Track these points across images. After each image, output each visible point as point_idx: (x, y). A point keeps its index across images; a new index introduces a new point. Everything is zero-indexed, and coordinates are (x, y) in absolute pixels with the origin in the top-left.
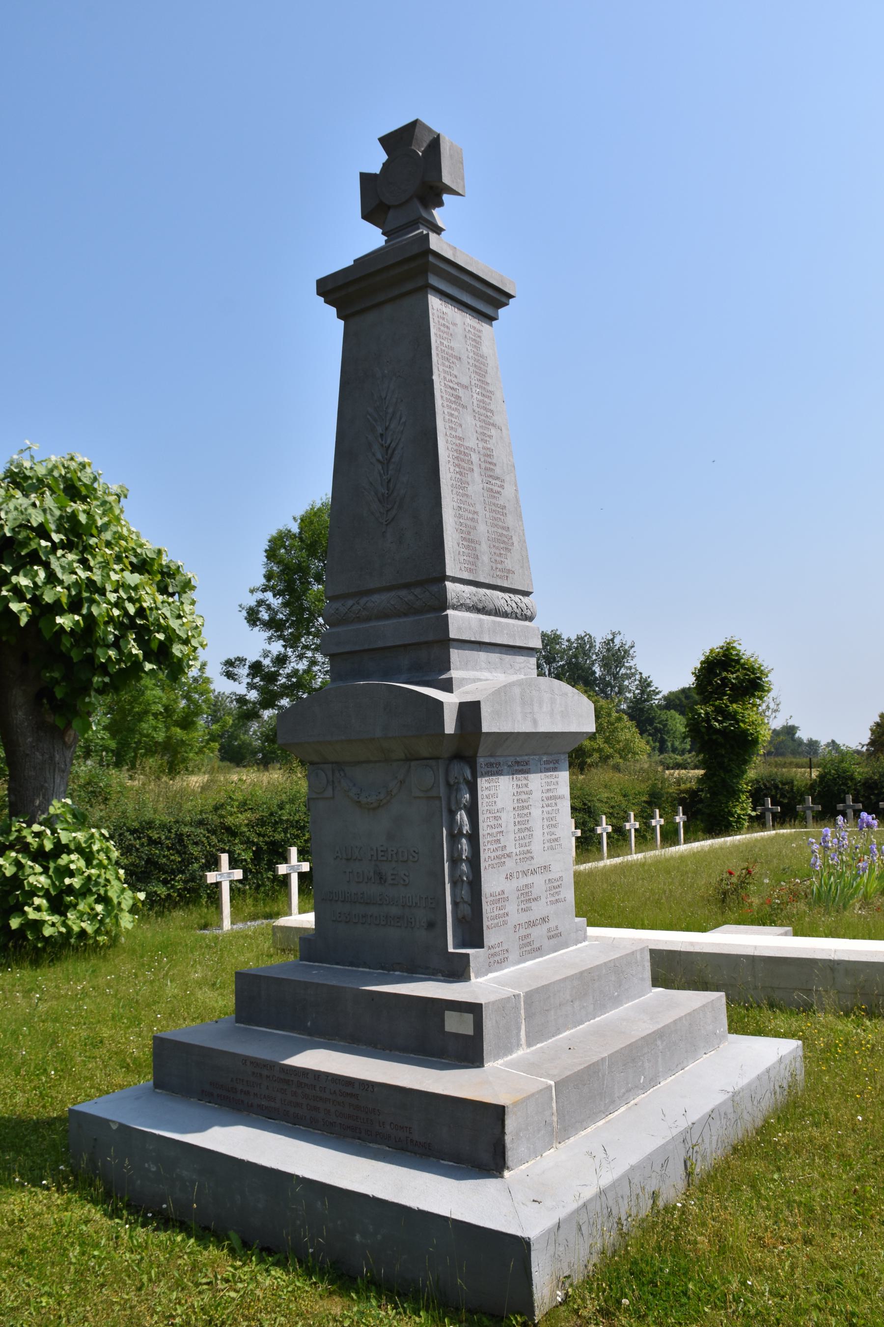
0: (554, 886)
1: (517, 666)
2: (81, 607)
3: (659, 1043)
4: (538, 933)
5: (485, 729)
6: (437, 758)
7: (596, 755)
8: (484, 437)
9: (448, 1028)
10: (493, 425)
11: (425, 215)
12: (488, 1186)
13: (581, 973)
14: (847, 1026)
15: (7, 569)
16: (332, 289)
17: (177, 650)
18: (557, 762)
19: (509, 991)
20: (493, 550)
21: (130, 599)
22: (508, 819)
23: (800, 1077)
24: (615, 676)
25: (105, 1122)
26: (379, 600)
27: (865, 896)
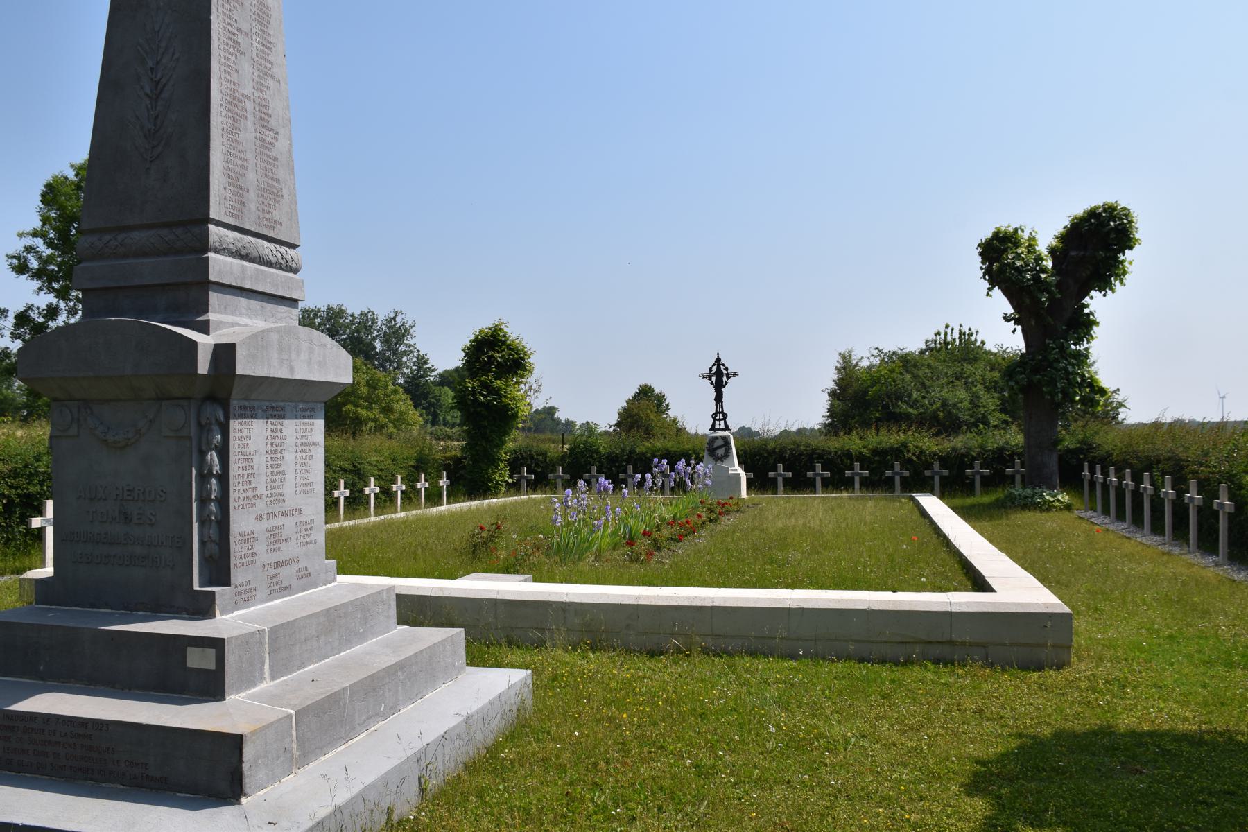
0: (305, 529)
1: (279, 316)
3: (400, 673)
4: (287, 573)
5: (239, 371)
6: (189, 398)
7: (371, 424)
8: (260, 87)
9: (189, 664)
10: (272, 77)
13: (328, 610)
14: (573, 658)
18: (313, 410)
19: (255, 627)
20: (262, 199)
22: (260, 461)
23: (529, 701)
24: (395, 352)
27: (599, 550)
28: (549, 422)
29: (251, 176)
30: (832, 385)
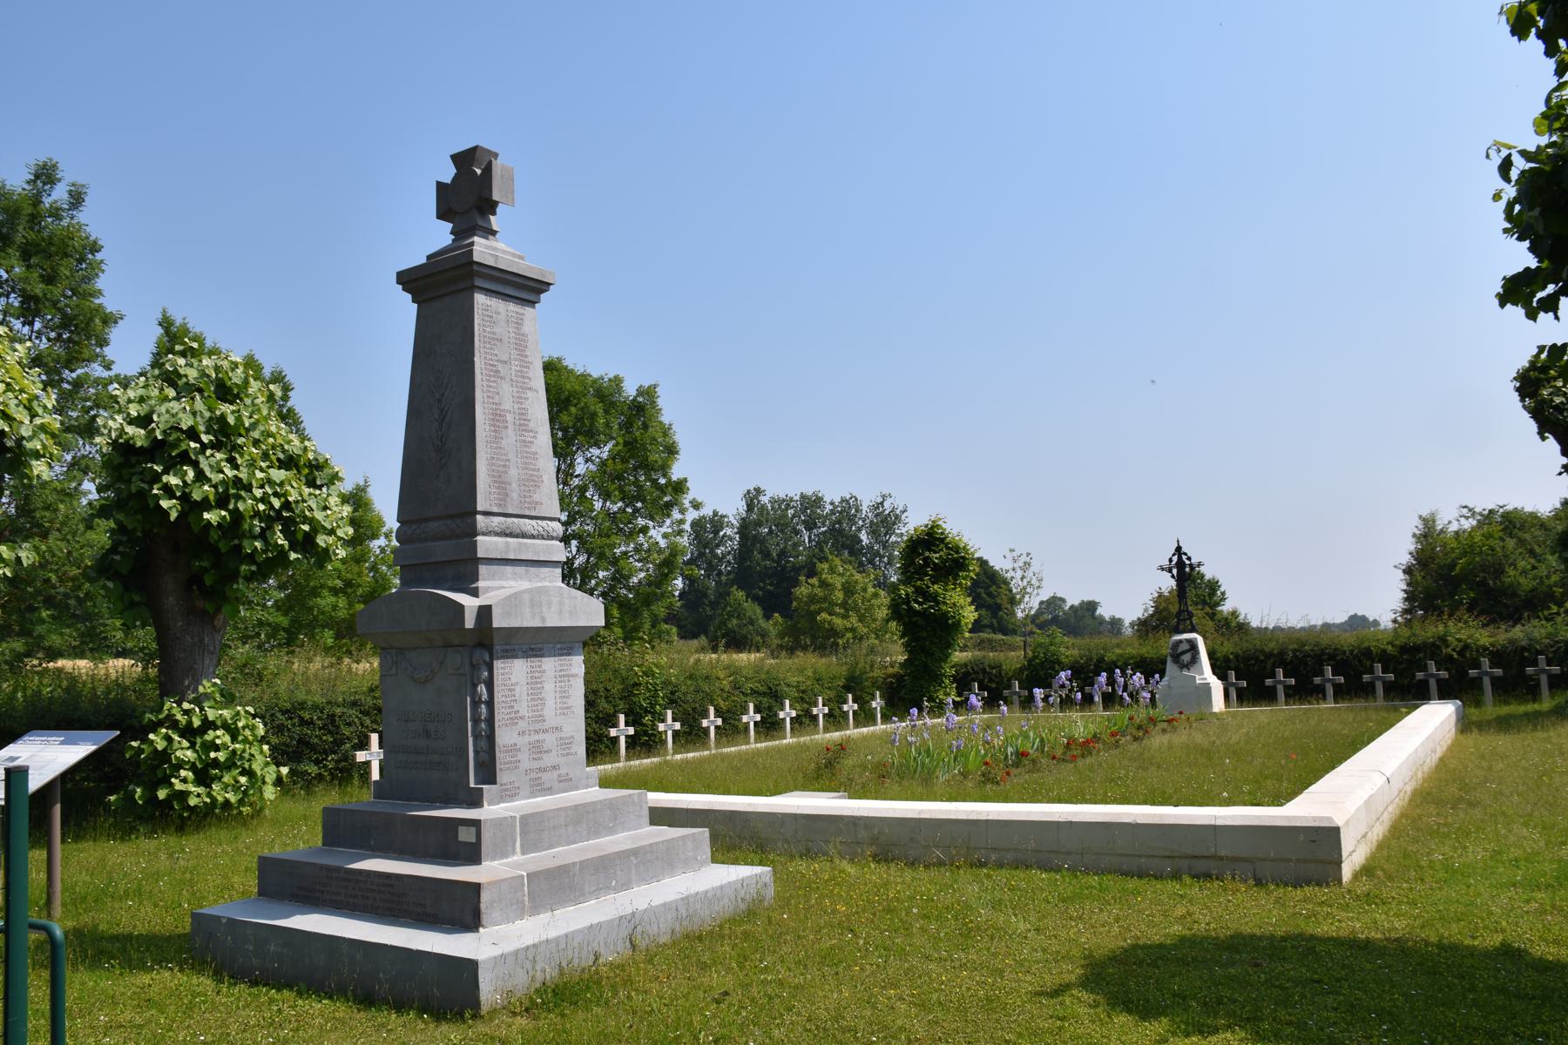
0: (566, 743)
2: (228, 503)
5: (495, 625)
11: (480, 223)
12: (467, 938)
15: (159, 468)
16: (408, 280)
17: (321, 540)
21: (276, 494)
22: (521, 691)
24: (885, 545)
25: (219, 918)
26: (433, 526)
28: (1089, 621)
29: (513, 472)
30: (1406, 559)
